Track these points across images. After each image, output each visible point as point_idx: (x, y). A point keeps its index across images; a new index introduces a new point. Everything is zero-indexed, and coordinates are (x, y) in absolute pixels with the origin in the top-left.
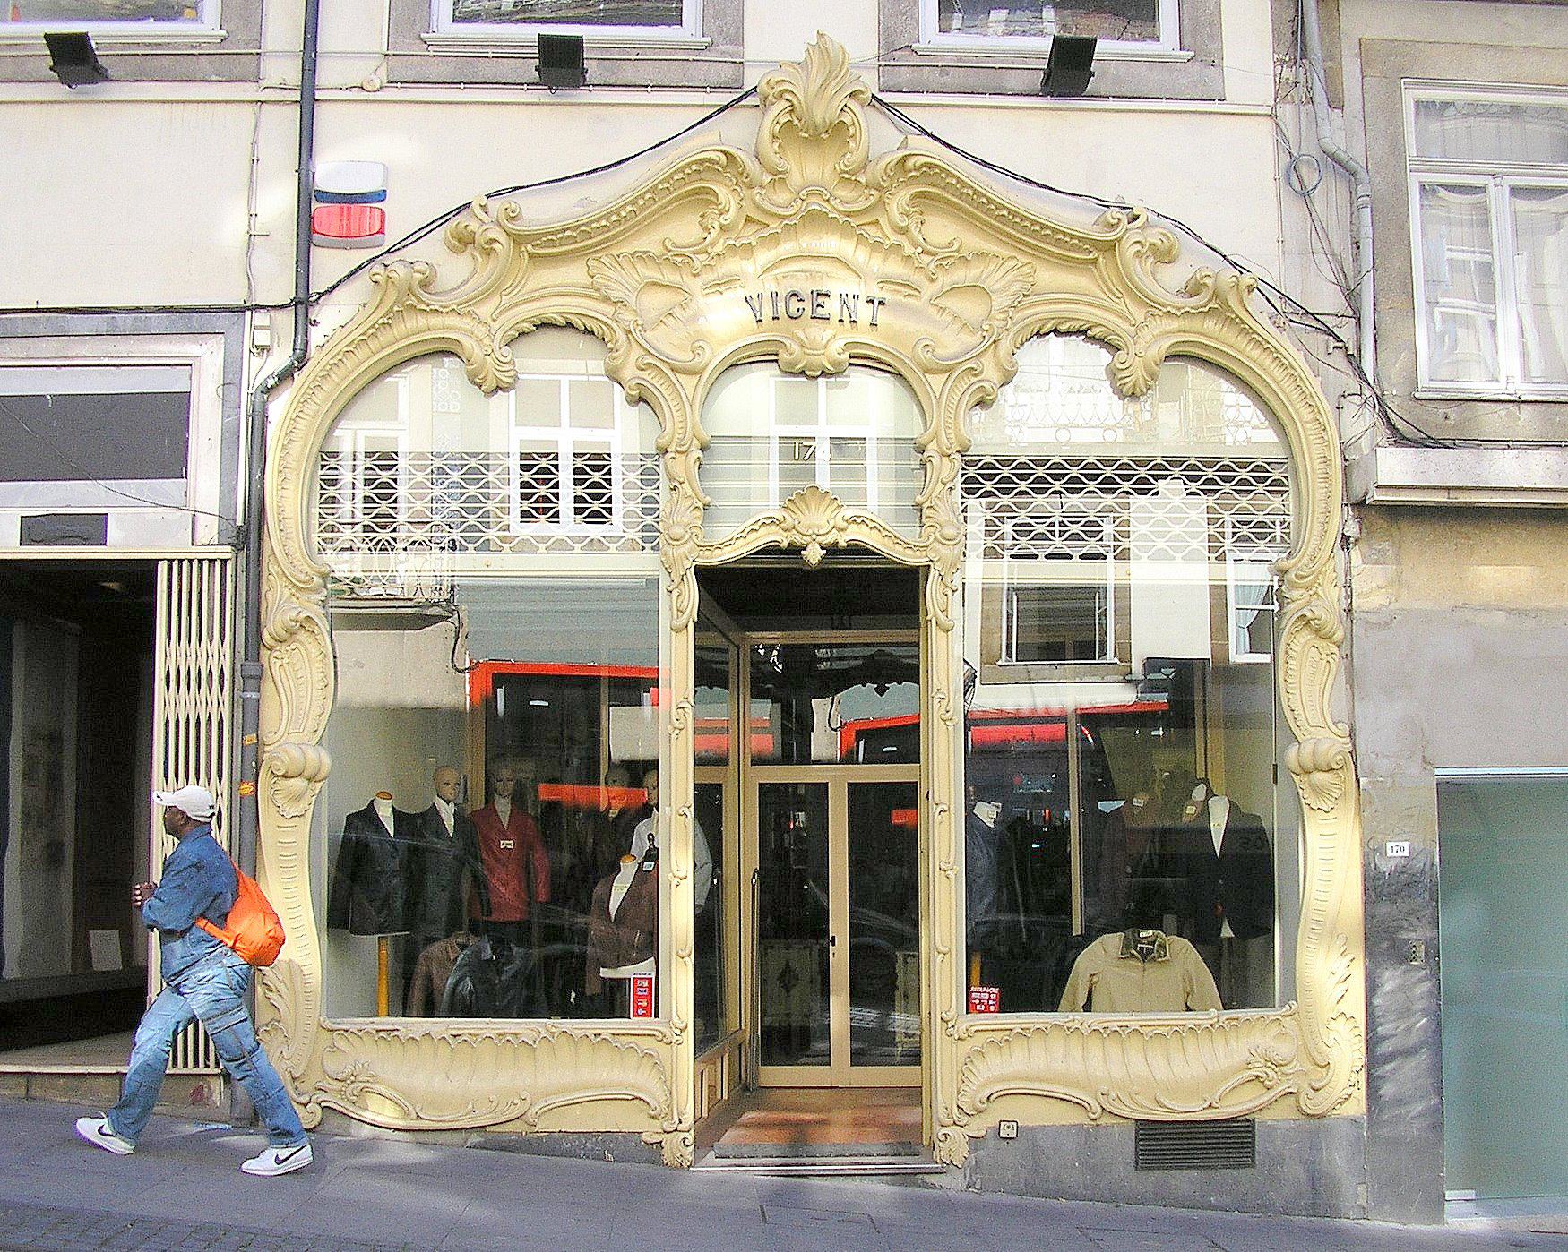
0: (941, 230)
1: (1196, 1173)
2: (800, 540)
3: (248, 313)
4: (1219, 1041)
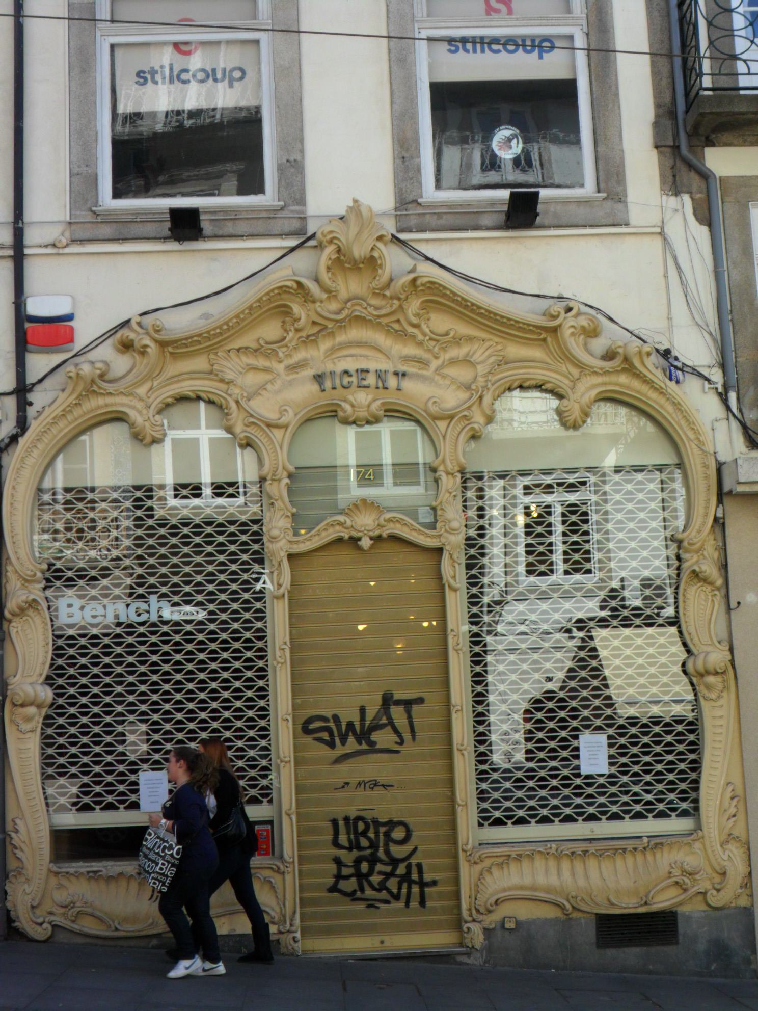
0: (440, 322)
4: (552, 863)
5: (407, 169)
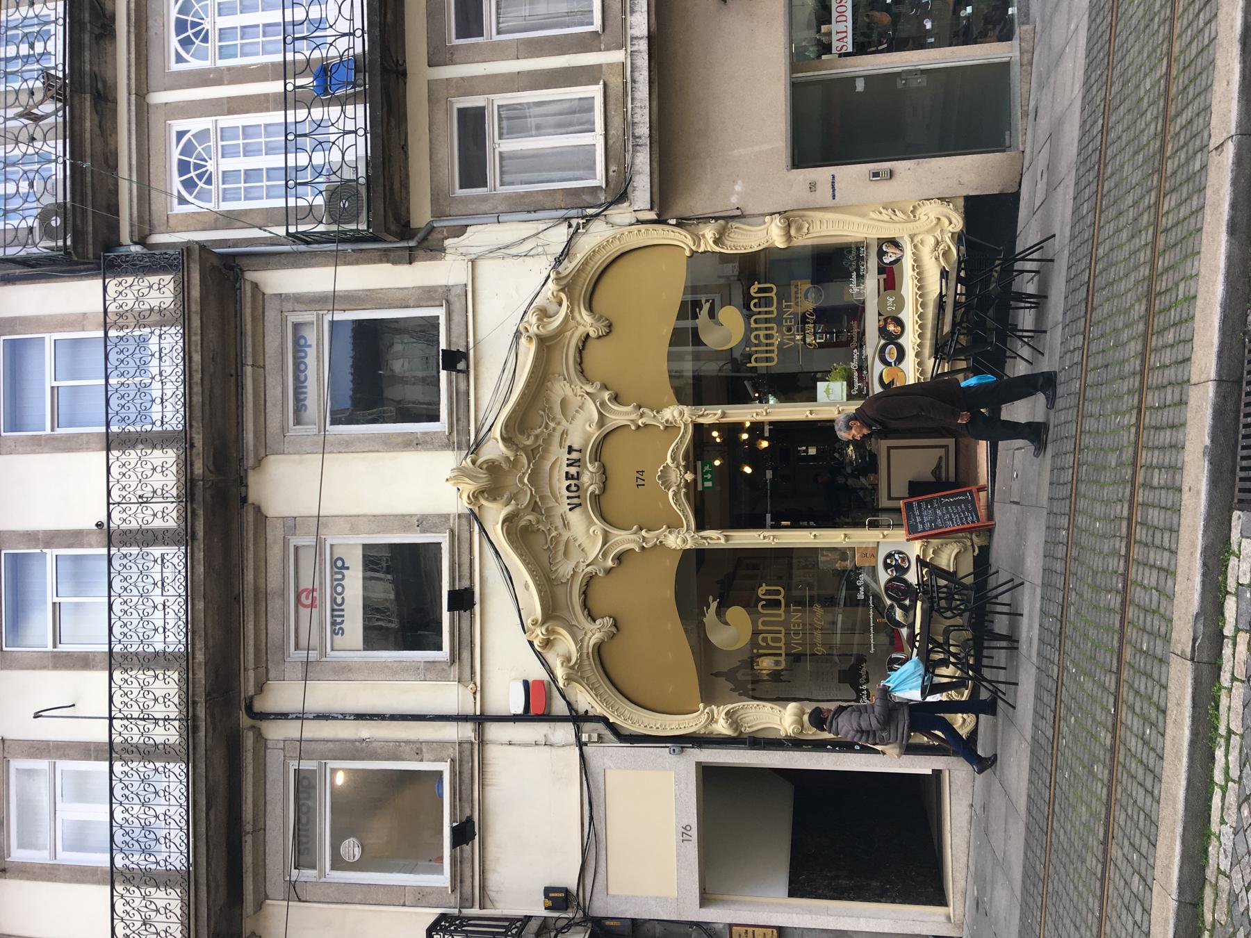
5: (425, 442)
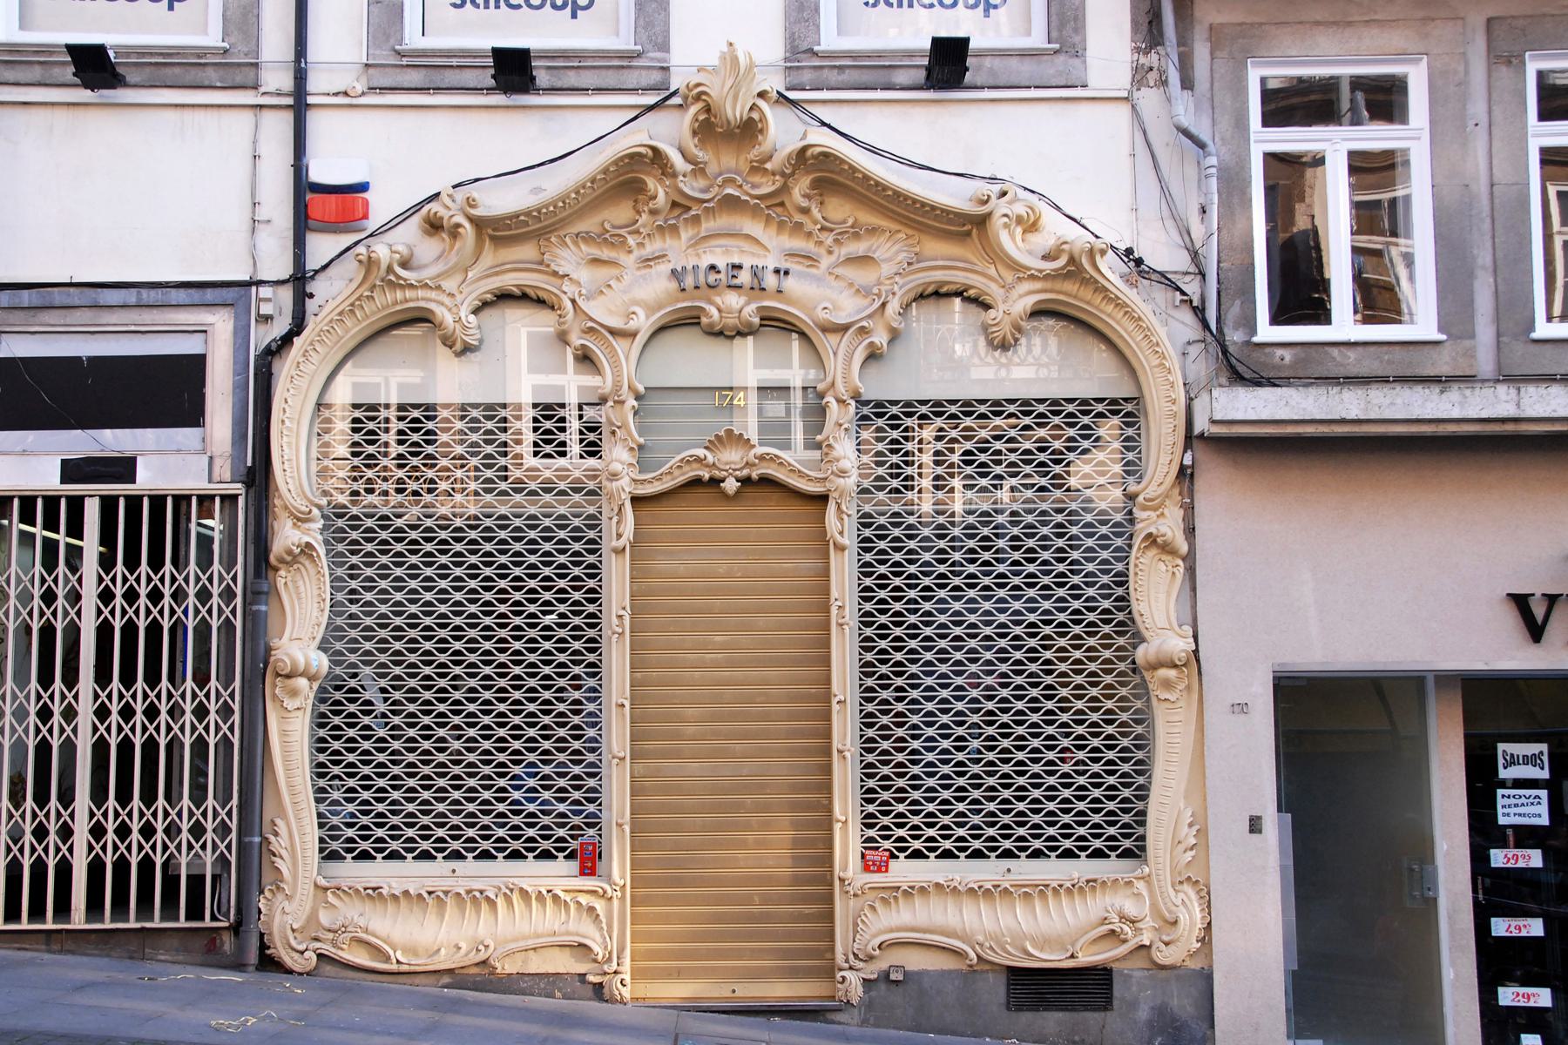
0: (840, 210)
1: (1060, 1014)
2: (717, 474)
3: (254, 289)
